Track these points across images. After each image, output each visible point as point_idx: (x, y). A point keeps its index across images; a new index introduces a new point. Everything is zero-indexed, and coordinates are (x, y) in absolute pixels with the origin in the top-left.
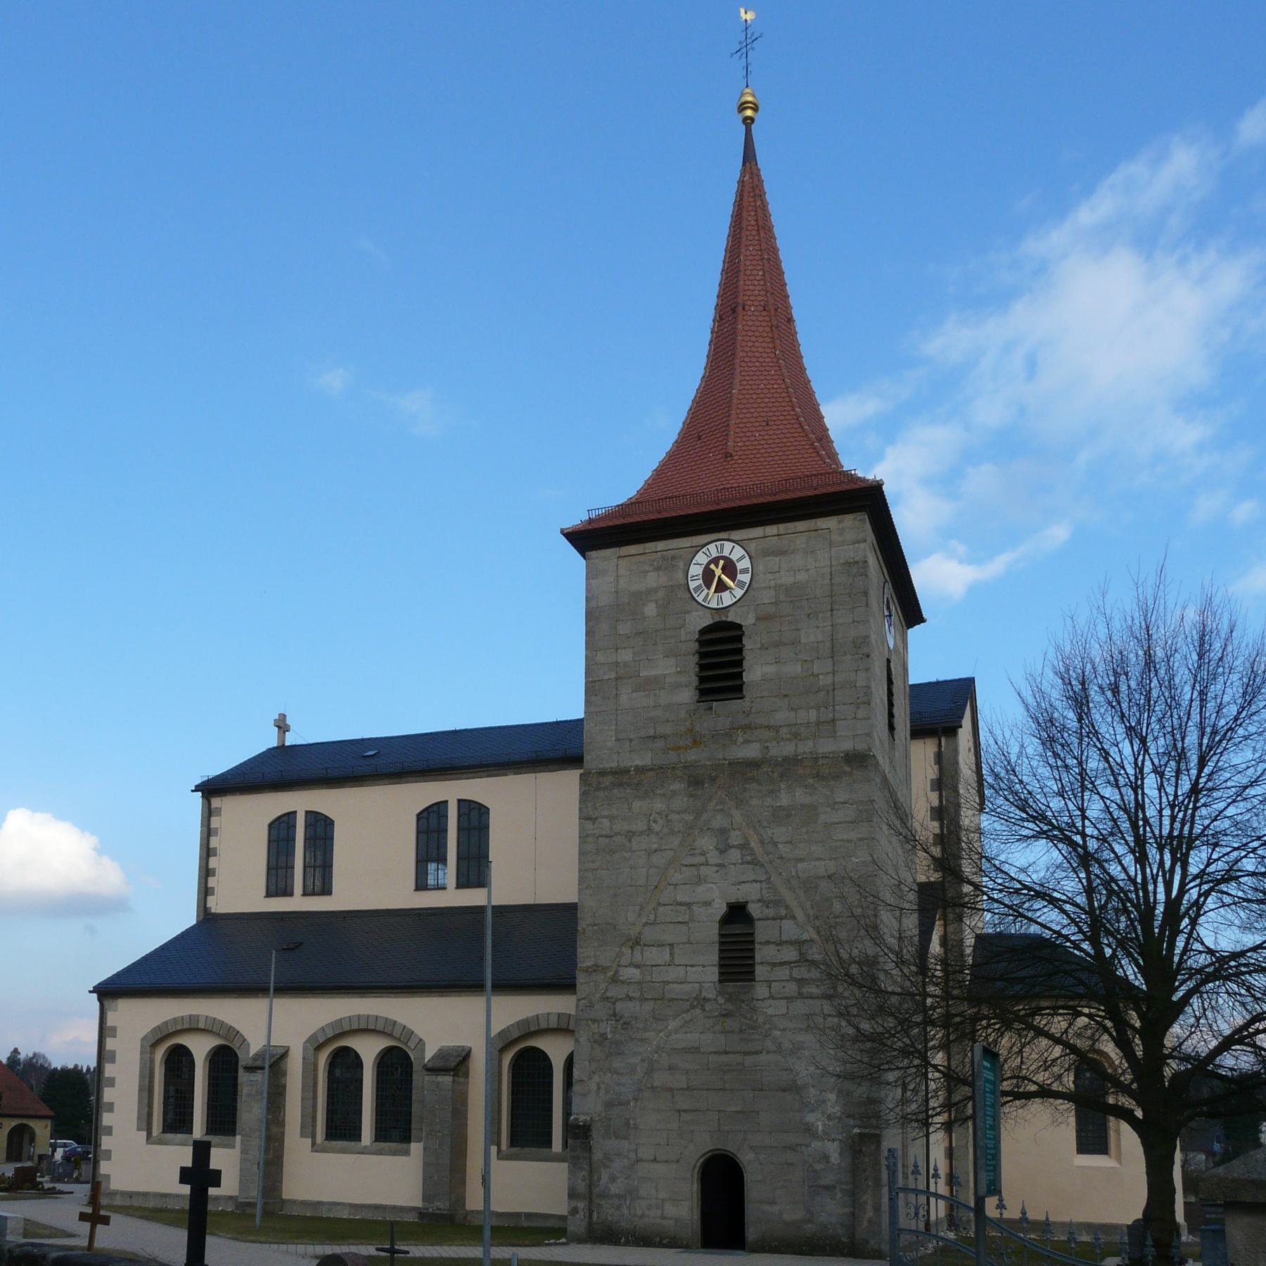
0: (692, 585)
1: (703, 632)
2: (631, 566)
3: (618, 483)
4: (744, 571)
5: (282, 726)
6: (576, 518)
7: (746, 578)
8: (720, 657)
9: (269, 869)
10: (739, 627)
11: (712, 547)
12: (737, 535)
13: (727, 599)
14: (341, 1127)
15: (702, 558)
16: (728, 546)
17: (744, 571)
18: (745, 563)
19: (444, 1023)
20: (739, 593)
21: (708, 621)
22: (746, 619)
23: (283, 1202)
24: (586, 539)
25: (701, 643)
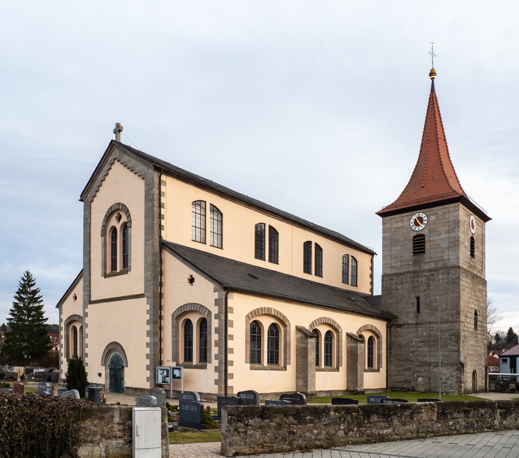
0: (411, 225)
1: (415, 237)
2: (397, 221)
3: (391, 196)
4: (425, 220)
5: (118, 130)
6: (379, 209)
7: (426, 222)
8: (419, 243)
9: (146, 229)
10: (424, 235)
11: (417, 214)
12: (422, 211)
13: (421, 228)
14: (254, 358)
15: (414, 217)
16: (421, 214)
17: (425, 220)
18: (426, 218)
19: (300, 316)
20: (424, 226)
21: (415, 234)
22: (426, 232)
23: (88, 384)
24: (383, 214)
25: (414, 241)
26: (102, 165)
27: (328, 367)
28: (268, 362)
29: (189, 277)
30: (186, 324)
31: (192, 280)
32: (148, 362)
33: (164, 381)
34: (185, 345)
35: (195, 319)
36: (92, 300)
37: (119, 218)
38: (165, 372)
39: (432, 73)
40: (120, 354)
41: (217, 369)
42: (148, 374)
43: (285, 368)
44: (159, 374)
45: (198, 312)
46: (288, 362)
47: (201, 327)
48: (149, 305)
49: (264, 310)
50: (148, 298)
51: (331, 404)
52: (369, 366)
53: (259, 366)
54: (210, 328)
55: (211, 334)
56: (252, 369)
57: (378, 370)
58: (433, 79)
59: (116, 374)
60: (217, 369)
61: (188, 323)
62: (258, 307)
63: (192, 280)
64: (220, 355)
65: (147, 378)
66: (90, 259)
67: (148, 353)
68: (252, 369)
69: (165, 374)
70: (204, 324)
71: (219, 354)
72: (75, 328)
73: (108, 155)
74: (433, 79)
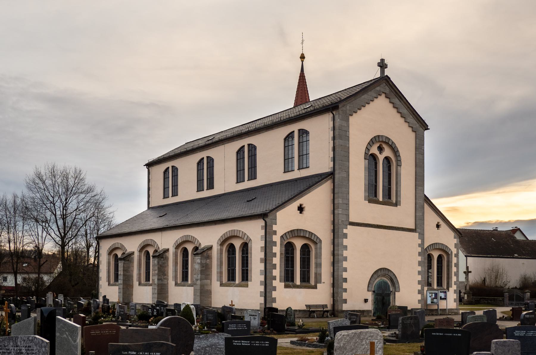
27: (304, 284)
28: (301, 281)
30: (244, 247)
31: (438, 226)
33: (432, 303)
34: (229, 267)
36: (261, 223)
38: (433, 295)
39: (303, 57)
42: (274, 294)
43: (315, 287)
44: (428, 296)
45: (241, 238)
47: (243, 251)
50: (419, 234)
52: (438, 285)
54: (452, 263)
55: (452, 267)
58: (302, 61)
59: (383, 298)
61: (232, 246)
65: (419, 300)
67: (420, 279)
69: (433, 296)
70: (245, 247)
73: (408, 107)
74: (302, 61)
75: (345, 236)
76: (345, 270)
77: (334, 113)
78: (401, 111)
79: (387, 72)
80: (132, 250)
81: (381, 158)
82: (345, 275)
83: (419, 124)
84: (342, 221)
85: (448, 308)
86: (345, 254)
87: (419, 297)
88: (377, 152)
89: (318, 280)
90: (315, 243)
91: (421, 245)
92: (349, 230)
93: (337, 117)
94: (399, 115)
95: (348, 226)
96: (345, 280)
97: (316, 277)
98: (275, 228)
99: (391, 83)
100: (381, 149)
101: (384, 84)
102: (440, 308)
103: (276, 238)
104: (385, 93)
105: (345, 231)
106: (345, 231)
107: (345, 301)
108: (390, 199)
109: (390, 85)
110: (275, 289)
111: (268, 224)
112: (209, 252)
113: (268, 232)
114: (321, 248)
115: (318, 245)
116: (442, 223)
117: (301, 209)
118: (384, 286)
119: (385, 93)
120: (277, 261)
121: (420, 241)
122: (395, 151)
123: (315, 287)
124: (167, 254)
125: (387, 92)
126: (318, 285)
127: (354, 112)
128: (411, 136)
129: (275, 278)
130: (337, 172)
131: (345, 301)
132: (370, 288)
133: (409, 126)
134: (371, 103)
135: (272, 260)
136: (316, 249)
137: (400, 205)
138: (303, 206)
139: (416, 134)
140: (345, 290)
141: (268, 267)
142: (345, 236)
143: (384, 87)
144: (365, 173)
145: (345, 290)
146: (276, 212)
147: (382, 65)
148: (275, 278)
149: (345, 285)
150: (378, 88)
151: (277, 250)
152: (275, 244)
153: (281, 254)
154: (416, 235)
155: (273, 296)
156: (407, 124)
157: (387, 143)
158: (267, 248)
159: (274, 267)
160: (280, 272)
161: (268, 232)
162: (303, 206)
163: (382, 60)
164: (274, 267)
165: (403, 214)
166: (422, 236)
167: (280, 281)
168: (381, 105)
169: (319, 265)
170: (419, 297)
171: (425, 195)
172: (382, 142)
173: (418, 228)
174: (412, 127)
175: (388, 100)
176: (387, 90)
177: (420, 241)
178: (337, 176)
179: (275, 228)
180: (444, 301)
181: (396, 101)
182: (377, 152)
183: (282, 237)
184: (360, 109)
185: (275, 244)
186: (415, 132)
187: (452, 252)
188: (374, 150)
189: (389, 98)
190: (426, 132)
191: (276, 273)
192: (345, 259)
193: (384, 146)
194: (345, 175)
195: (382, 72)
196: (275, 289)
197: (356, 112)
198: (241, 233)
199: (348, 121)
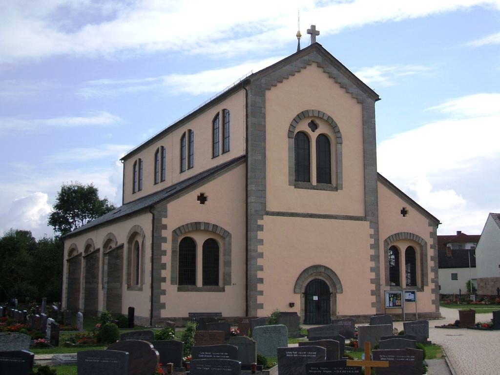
26: (326, 56)
29: (402, 209)
31: (404, 212)
32: (260, 287)
35: (200, 240)
37: (314, 126)
40: (324, 280)
41: (433, 291)
42: (163, 299)
43: (223, 290)
46: (425, 283)
48: (373, 230)
49: (400, 236)
50: (371, 222)
51: (37, 357)
53: (216, 287)
55: (427, 261)
56: (179, 290)
57: (141, 289)
60: (433, 291)
62: (399, 232)
63: (404, 212)
64: (436, 279)
66: (377, 197)
68: (179, 290)
71: (435, 278)
72: (137, 242)
75: (261, 228)
76: (261, 269)
77: (247, 88)
78: (339, 81)
79: (318, 39)
80: (81, 251)
81: (314, 136)
82: (260, 274)
83: (367, 97)
84: (256, 211)
85: (418, 311)
86: (260, 249)
87: (373, 299)
88: (308, 130)
89: (228, 281)
90: (223, 238)
91: (376, 236)
92: (266, 221)
93: (249, 92)
94: (337, 86)
95: (264, 216)
96: (261, 281)
97: (224, 279)
98: (164, 221)
99: (323, 51)
100: (314, 126)
101: (315, 53)
102: (406, 311)
103: (167, 234)
104: (317, 63)
105: (260, 222)
106: (260, 222)
107: (261, 306)
108: (326, 178)
109: (322, 53)
110: (164, 292)
111: (155, 217)
112: (119, 251)
113: (157, 227)
114: (230, 244)
115: (227, 239)
116: (409, 208)
117: (202, 199)
118: (319, 288)
119: (317, 63)
120: (167, 259)
121: (372, 232)
122: (331, 123)
123: (223, 290)
124: (97, 254)
125: (319, 61)
126: (227, 287)
127: (272, 85)
128: (355, 110)
129: (164, 280)
130: (249, 154)
131: (261, 306)
132: (297, 290)
133: (358, 103)
134: (297, 74)
135: (161, 259)
136: (224, 244)
137: (342, 189)
138: (205, 196)
139: (363, 106)
140: (261, 293)
141: (155, 267)
142: (261, 228)
143: (314, 55)
144: (289, 154)
145: (261, 293)
146: (167, 203)
147: (313, 32)
148: (164, 280)
149: (260, 287)
150: (306, 58)
151: (167, 247)
152: (165, 240)
153: (173, 252)
154: (366, 224)
155: (161, 302)
156: (349, 96)
157: (318, 117)
158: (154, 245)
159: (164, 266)
160: (172, 272)
161: (157, 227)
162: (205, 196)
163: (313, 27)
164: (164, 266)
165: (348, 197)
166: (375, 224)
167: (172, 283)
168: (312, 74)
169: (228, 264)
170: (373, 299)
171: (378, 173)
172: (314, 119)
173: (370, 214)
174: (357, 98)
175: (321, 70)
176: (320, 59)
177: (372, 232)
178: (249, 159)
179: (164, 221)
180: (414, 303)
181: (333, 70)
182: (308, 130)
183: (174, 231)
184: (281, 82)
185: (165, 240)
186: (362, 103)
187: (426, 243)
188: (304, 126)
189: (323, 68)
190: (377, 103)
191: (166, 273)
192: (261, 255)
193: (317, 121)
194: (260, 158)
195: (313, 38)
196: (164, 292)
197: (276, 86)
198: (409, 235)
199: (263, 96)
